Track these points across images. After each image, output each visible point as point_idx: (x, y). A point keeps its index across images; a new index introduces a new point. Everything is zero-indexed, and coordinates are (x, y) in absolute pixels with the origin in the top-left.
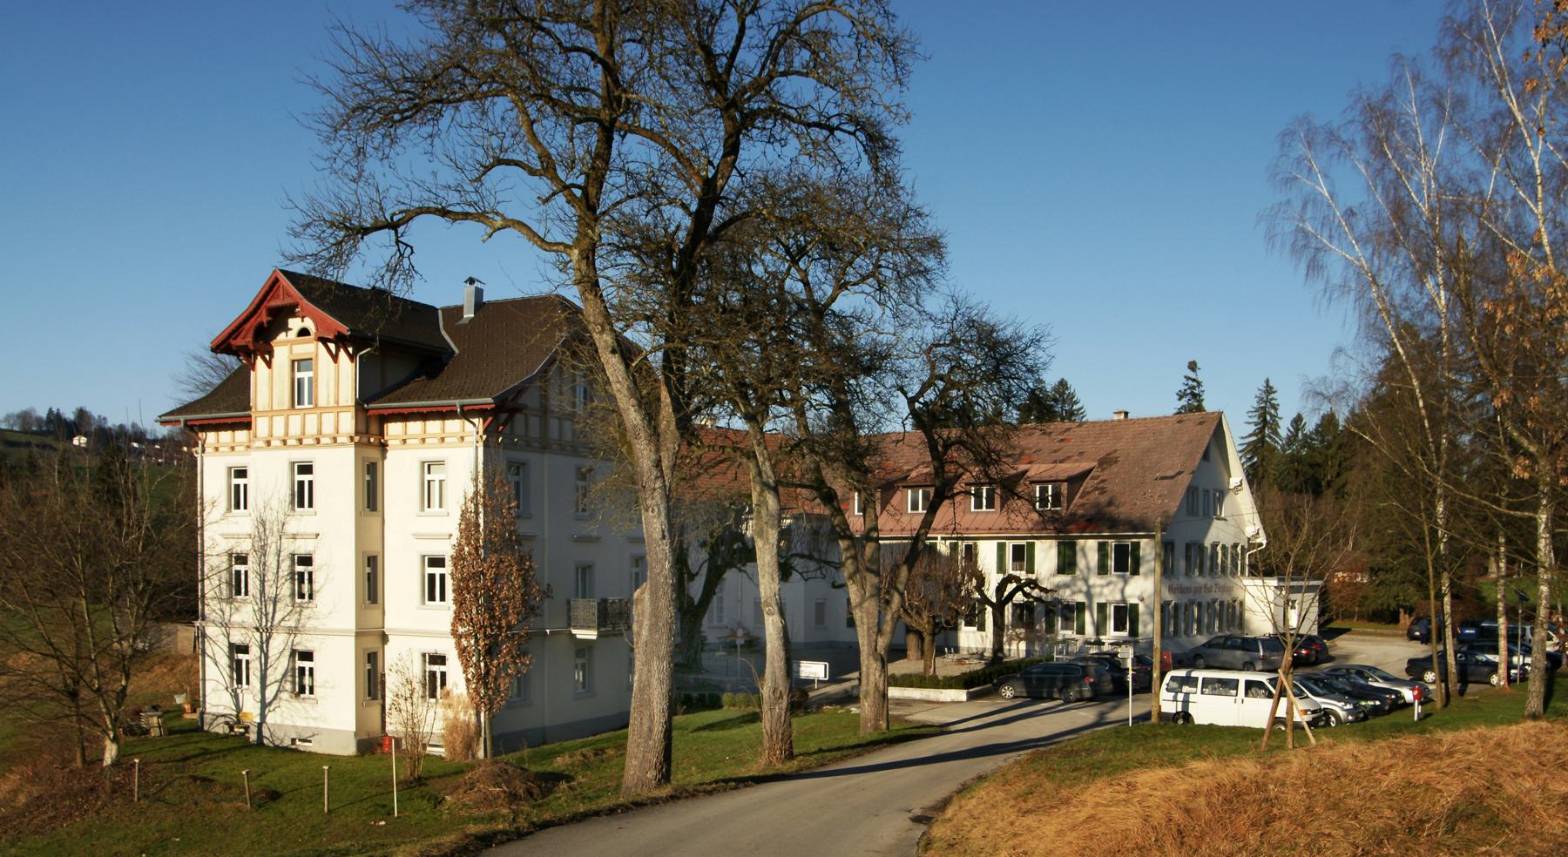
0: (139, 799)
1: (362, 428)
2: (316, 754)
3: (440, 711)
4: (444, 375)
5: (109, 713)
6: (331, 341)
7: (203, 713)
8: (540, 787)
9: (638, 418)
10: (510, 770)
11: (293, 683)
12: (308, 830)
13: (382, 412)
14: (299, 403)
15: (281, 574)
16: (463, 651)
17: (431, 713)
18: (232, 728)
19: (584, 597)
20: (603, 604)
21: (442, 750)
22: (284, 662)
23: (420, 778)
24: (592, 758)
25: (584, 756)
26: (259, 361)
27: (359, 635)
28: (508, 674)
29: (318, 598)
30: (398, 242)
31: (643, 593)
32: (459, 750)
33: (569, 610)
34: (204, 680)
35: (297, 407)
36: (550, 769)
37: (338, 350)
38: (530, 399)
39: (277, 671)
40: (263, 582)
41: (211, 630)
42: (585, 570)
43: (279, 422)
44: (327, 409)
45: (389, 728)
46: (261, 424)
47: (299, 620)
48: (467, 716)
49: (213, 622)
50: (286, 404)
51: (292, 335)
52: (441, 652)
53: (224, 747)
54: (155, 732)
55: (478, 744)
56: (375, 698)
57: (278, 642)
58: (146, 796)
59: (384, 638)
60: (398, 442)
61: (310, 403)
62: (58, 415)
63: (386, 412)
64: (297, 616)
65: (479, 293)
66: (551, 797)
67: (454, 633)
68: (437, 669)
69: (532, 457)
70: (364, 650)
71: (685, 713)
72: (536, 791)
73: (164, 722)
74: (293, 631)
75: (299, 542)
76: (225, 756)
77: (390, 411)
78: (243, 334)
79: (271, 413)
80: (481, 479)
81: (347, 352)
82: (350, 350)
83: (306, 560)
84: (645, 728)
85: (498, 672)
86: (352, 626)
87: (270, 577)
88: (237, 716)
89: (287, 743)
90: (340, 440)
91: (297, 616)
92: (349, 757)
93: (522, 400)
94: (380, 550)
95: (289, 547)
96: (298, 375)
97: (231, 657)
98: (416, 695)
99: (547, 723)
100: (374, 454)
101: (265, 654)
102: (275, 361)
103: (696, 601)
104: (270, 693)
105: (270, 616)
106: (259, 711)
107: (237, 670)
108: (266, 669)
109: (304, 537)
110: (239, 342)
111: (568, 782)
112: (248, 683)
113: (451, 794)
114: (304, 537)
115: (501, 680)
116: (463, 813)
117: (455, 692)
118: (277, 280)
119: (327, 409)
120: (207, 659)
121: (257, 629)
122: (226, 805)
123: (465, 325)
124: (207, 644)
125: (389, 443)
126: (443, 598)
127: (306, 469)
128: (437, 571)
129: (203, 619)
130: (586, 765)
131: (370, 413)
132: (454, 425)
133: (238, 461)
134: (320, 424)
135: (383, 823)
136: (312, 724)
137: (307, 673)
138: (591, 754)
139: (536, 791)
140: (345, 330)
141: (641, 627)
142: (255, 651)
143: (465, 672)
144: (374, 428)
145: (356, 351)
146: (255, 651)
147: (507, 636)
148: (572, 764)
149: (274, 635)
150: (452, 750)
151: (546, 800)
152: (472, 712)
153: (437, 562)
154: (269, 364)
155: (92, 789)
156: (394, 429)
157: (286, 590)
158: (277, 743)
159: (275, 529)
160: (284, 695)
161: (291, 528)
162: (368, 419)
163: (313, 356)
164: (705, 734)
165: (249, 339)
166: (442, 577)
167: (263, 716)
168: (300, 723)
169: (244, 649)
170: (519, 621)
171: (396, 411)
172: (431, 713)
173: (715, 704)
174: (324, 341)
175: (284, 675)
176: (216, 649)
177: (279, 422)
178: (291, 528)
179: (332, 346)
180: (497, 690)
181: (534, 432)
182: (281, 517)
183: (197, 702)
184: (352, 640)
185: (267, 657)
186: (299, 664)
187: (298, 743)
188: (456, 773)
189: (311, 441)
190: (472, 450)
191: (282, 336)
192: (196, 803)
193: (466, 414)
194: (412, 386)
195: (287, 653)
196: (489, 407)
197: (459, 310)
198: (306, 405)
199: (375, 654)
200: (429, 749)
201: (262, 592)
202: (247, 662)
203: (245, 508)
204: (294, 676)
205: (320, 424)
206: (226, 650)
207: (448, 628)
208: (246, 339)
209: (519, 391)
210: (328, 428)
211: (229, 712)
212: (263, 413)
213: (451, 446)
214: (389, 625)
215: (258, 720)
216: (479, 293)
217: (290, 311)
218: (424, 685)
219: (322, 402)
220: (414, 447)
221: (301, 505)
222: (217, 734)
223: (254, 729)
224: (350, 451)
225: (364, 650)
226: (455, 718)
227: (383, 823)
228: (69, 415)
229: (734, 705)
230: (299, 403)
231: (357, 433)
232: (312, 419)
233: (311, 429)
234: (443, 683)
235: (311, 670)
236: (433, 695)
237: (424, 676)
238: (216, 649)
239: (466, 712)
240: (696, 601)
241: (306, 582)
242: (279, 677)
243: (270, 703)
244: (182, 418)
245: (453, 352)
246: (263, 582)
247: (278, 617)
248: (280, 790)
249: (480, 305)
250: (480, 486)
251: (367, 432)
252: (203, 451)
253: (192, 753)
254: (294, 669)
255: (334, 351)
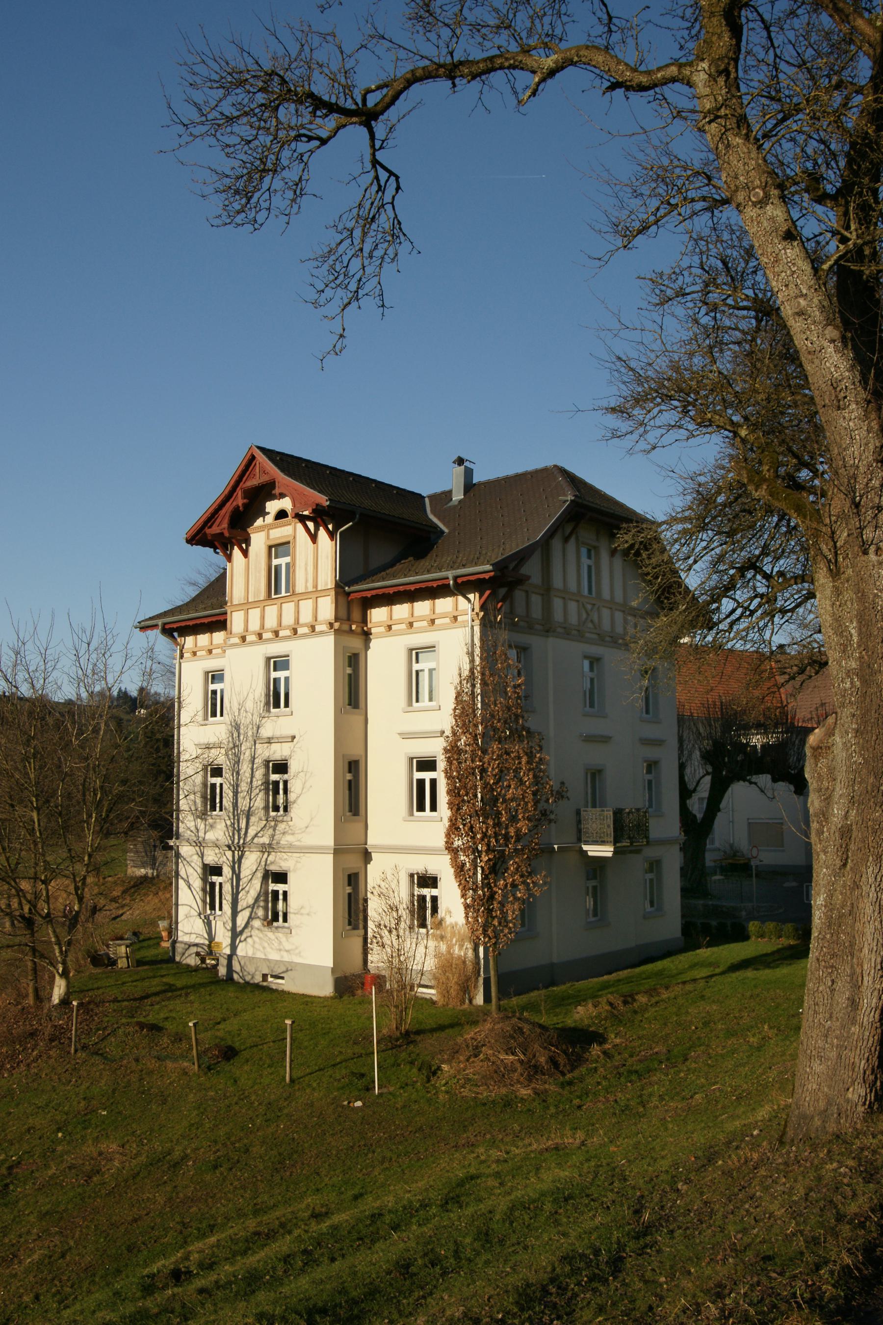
0: (76, 1051)
1: (343, 614)
2: (289, 993)
3: (432, 944)
4: (433, 553)
5: (59, 943)
6: (308, 518)
7: (174, 942)
8: (565, 1052)
9: (844, 365)
10: (526, 1028)
11: (266, 909)
12: (262, 1110)
13: (364, 594)
14: (276, 593)
15: (255, 784)
16: (459, 869)
17: (421, 950)
18: (203, 960)
19: (594, 806)
20: (618, 814)
21: (433, 991)
22: (256, 886)
23: (407, 1033)
24: (621, 1008)
25: (611, 1004)
26: (237, 552)
27: (338, 852)
28: (516, 899)
29: (294, 811)
30: (375, 163)
31: (830, 733)
32: (453, 993)
33: (579, 822)
34: (177, 905)
35: (273, 596)
36: (570, 1022)
37: (317, 529)
38: (532, 569)
39: (247, 897)
40: (236, 793)
41: (186, 850)
42: (595, 775)
43: (255, 614)
44: (306, 595)
45: (370, 966)
46: (236, 621)
47: (273, 836)
48: (464, 951)
49: (188, 840)
50: (263, 595)
51: (270, 519)
52: (432, 870)
53: (191, 981)
54: (122, 963)
55: (476, 987)
56: (356, 928)
57: (251, 862)
58: (85, 1047)
59: (367, 856)
60: (382, 629)
61: (287, 591)
62: (126, 693)
63: (369, 594)
64: (271, 831)
65: (469, 473)
66: (583, 1070)
67: (450, 848)
68: (427, 892)
69: (535, 642)
70: (343, 869)
71: (709, 945)
72: (562, 1060)
73: (132, 952)
74: (267, 849)
75: (274, 747)
76: (187, 995)
77: (374, 592)
78: (218, 520)
79: (247, 606)
80: (477, 651)
81: (327, 529)
82: (330, 527)
83: (281, 767)
84: (842, 999)
85: (505, 896)
86: (329, 841)
87: (244, 787)
88: (209, 946)
89: (258, 979)
90: (318, 628)
91: (271, 831)
92: (325, 998)
93: (525, 570)
94: (363, 753)
95: (264, 752)
96: (275, 562)
97: (204, 880)
98: (402, 925)
99: (555, 960)
100: (355, 643)
101: (237, 875)
102: (252, 549)
103: (699, 816)
104: (241, 920)
105: (243, 832)
106: (229, 941)
107: (210, 895)
108: (238, 893)
109: (280, 740)
110: (215, 530)
111: (600, 1044)
112: (221, 909)
113: (449, 1062)
114: (280, 740)
115: (509, 906)
116: (465, 1092)
117: (449, 921)
118: (253, 458)
119: (306, 595)
120: (181, 882)
121: (229, 847)
122: (170, 1064)
123: (455, 506)
124: (181, 865)
125: (373, 631)
126: (434, 808)
127: (280, 663)
128: (427, 776)
129: (177, 838)
130: (615, 1017)
131: (352, 596)
132: (445, 604)
133: (212, 664)
134: (298, 612)
135: (359, 1104)
136: (286, 958)
137: (281, 897)
138: (619, 1002)
139: (562, 1060)
140: (324, 500)
141: (828, 800)
142: (227, 871)
143: (463, 896)
144: (356, 614)
145: (336, 528)
146: (227, 871)
147: (516, 850)
148: (598, 1016)
149: (464, 922)
150: (445, 992)
151: (576, 1073)
152: (469, 945)
153: (427, 765)
154: (245, 553)
155: (32, 1034)
156: (378, 615)
157: (259, 803)
158: (248, 978)
159: (250, 734)
160: (257, 923)
161: (266, 732)
162: (349, 604)
163: (291, 539)
164: (750, 973)
165: (225, 525)
166: (433, 782)
167: (233, 947)
168: (274, 956)
169: (217, 870)
170: (530, 831)
171: (380, 592)
172: (421, 950)
173: (740, 935)
174: (302, 519)
175: (257, 900)
176: (190, 870)
177: (255, 614)
178: (266, 732)
179: (311, 525)
180: (504, 920)
181: (537, 612)
182: (256, 719)
183: (172, 930)
184: (331, 857)
185: (238, 879)
186: (272, 887)
187: (270, 979)
188: (452, 1026)
189: (287, 633)
190: (468, 630)
191: (259, 522)
192: (137, 1060)
193: (462, 588)
194: (398, 567)
195: (260, 875)
196: (487, 576)
197: (448, 494)
198: (283, 594)
199: (356, 875)
200: (421, 990)
201: (235, 805)
202: (221, 884)
203: (222, 715)
204: (266, 901)
205: (298, 612)
206: (199, 870)
207: (440, 841)
208: (221, 526)
209: (522, 557)
210: (306, 617)
211: (198, 941)
212: (240, 607)
213: (444, 628)
214: (373, 839)
215: (228, 951)
216: (469, 473)
217: (267, 491)
218: (412, 912)
219: (300, 588)
220: (400, 633)
221: (277, 705)
222: (188, 966)
223: (223, 962)
224: (329, 641)
225: (343, 869)
226: (449, 952)
227: (359, 1104)
228: (134, 693)
229: (762, 936)
230: (276, 593)
231: (337, 619)
232: (289, 609)
233: (288, 619)
234: (435, 910)
235: (285, 893)
236: (423, 925)
237: (412, 902)
238: (190, 870)
239: (461, 947)
240: (699, 816)
241: (281, 792)
242: (251, 901)
243: (242, 932)
244: (160, 622)
245: (442, 532)
246: (236, 793)
247: (252, 832)
248: (237, 1045)
249: (469, 486)
250: (477, 660)
251: (349, 619)
252: (182, 657)
253: (154, 990)
254: (266, 893)
255: (312, 530)
